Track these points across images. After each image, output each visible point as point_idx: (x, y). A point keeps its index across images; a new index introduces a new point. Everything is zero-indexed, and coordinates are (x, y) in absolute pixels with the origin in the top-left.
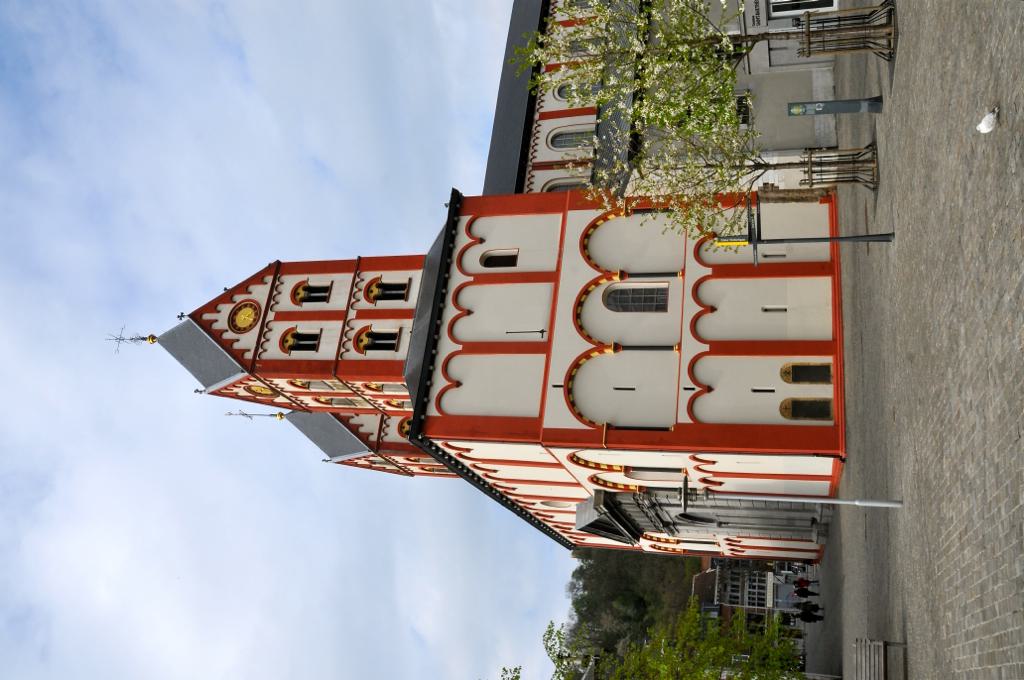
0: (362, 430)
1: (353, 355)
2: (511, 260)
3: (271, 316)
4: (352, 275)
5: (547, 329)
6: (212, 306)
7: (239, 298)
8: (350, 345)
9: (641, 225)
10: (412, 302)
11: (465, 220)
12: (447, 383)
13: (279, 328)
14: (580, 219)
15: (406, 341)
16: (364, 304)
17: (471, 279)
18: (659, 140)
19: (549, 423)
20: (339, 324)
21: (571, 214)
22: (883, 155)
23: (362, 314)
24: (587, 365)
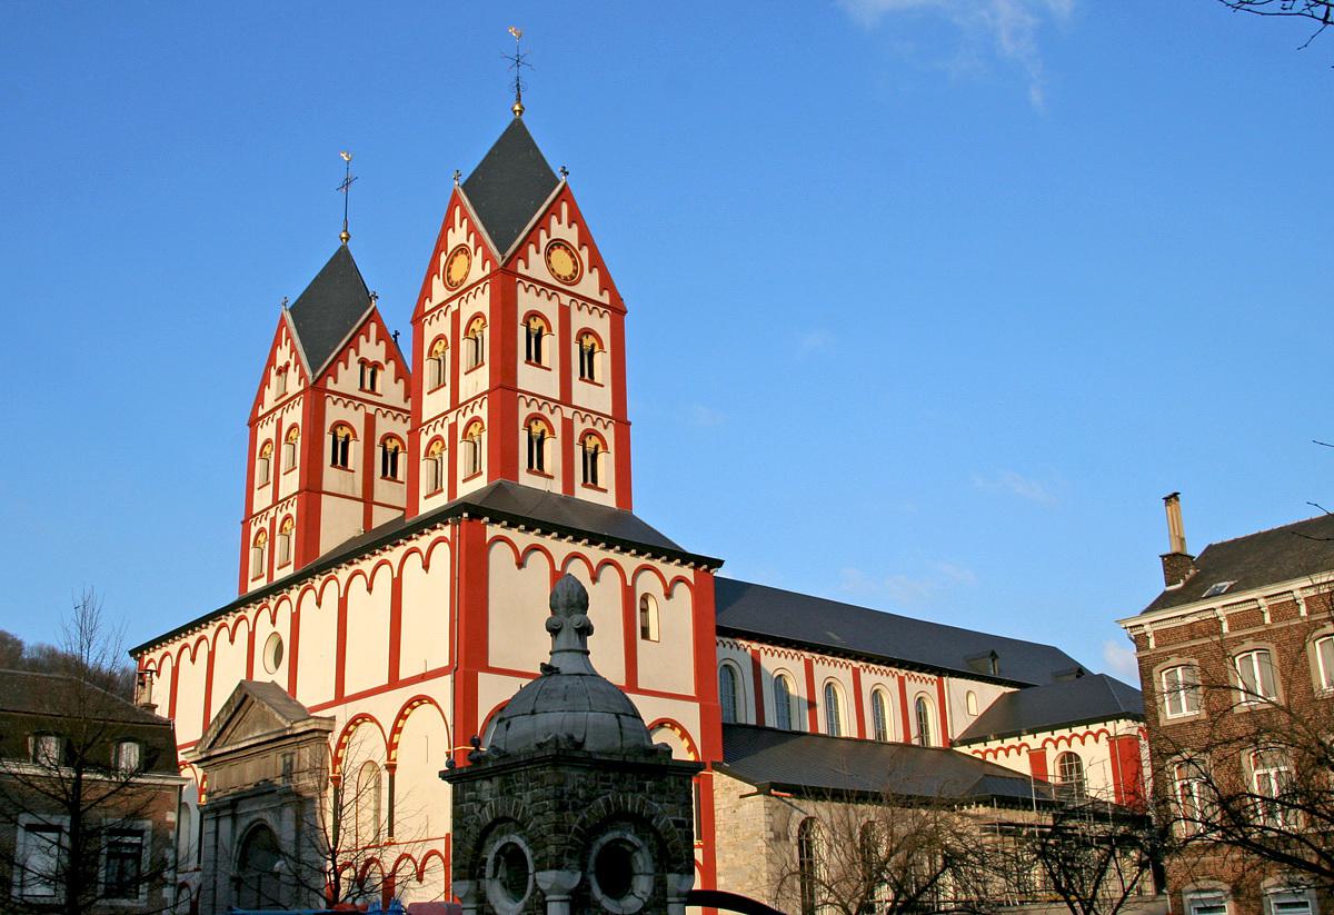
1: (524, 412)
2: (645, 634)
3: (566, 299)
6: (575, 218)
7: (584, 254)
8: (534, 409)
9: (427, 737)
10: (583, 494)
11: (688, 572)
12: (521, 550)
13: (550, 310)
16: (579, 428)
17: (629, 583)
18: (891, 850)
21: (696, 706)
23: (568, 425)
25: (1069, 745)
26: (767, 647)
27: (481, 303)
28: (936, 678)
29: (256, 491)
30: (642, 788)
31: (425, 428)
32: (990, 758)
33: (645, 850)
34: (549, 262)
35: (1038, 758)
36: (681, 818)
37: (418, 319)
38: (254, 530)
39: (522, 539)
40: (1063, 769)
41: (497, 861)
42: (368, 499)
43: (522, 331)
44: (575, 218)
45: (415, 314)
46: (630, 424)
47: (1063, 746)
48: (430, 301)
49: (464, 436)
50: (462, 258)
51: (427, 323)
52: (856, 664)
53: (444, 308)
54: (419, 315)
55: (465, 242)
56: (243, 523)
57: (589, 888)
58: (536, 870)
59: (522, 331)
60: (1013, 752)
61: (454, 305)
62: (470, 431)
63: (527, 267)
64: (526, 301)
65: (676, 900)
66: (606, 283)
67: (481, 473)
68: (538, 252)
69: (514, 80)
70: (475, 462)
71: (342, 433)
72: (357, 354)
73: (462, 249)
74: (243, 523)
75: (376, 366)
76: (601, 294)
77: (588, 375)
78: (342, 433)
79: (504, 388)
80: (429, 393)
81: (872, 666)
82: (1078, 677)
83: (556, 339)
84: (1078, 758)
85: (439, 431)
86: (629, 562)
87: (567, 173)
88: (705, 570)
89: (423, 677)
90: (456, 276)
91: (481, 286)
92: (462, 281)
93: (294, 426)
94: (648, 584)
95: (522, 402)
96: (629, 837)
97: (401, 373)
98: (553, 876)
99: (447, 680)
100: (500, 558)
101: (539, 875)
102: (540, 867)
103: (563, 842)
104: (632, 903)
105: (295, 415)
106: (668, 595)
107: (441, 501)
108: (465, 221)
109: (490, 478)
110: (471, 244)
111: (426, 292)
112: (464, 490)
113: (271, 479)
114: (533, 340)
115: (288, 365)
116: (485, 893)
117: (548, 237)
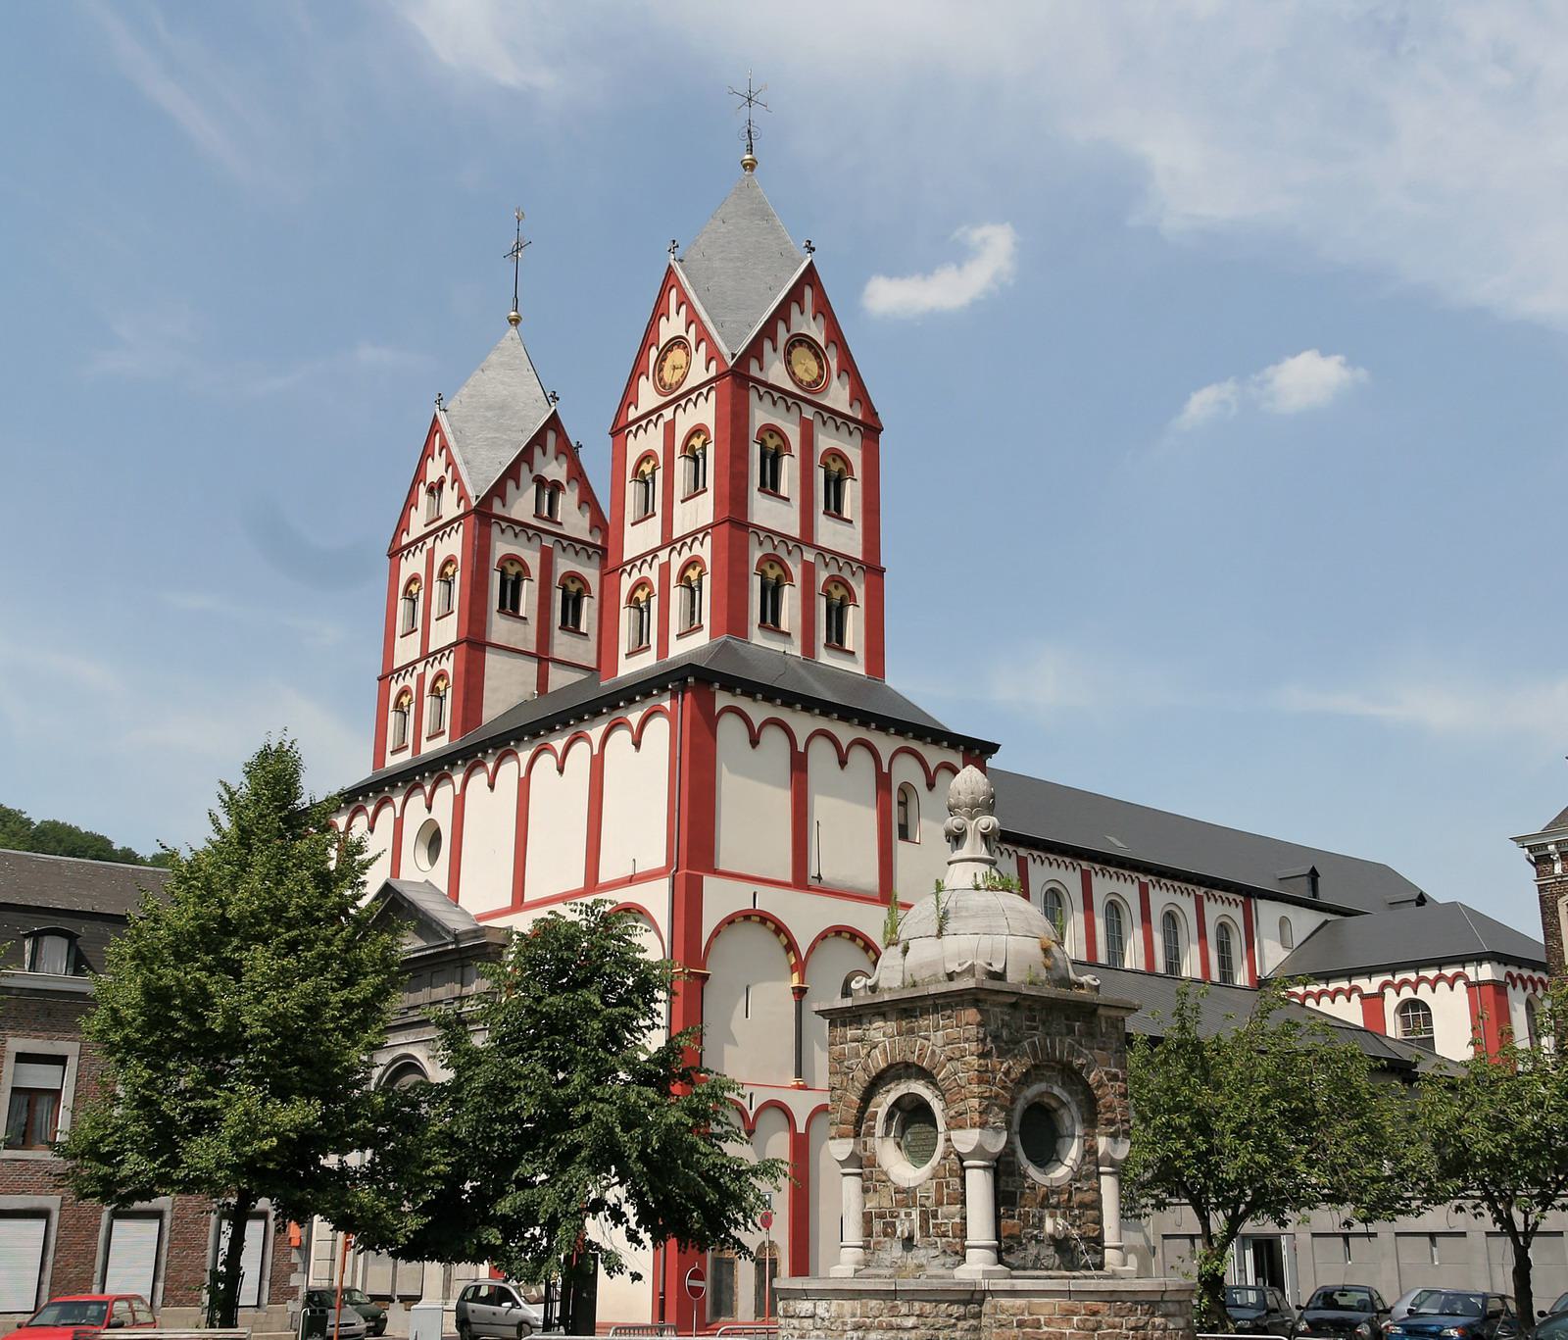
0: (511, 485)
1: (756, 554)
2: (904, 835)
3: (548, 542)
4: (860, 557)
5: (822, 885)
6: (824, 309)
15: (776, 645)
16: (822, 576)
19: (710, 883)
20: (795, 532)
23: (809, 570)
24: (776, 945)
25: (1416, 992)
26: (1036, 853)
27: (705, 412)
28: (1242, 899)
29: (398, 639)
30: (1071, 1031)
31: (628, 568)
32: (1310, 1003)
33: (1074, 1108)
34: (788, 363)
35: (1373, 1003)
36: (1114, 1070)
37: (620, 430)
38: (395, 689)
39: (759, 712)
40: (1405, 1022)
41: (890, 1116)
42: (543, 657)
45: (616, 420)
46: (883, 570)
47: (1407, 993)
48: (636, 408)
49: (396, 706)
50: (677, 356)
51: (631, 436)
52: (1144, 879)
53: (654, 418)
54: (620, 426)
55: (684, 335)
56: (380, 679)
57: (1014, 1152)
58: (949, 1127)
60: (1341, 999)
61: (668, 413)
62: (446, 570)
63: (761, 369)
64: (761, 415)
65: (1110, 1169)
67: (700, 627)
68: (775, 350)
69: (744, 123)
70: (692, 614)
71: (513, 570)
72: (531, 471)
73: (678, 342)
74: (380, 679)
75: (556, 487)
77: (834, 509)
78: (513, 570)
79: (733, 521)
80: (633, 525)
81: (1163, 881)
82: (1418, 904)
83: (797, 461)
84: (1427, 1008)
85: (646, 571)
86: (886, 744)
87: (814, 249)
88: (977, 756)
89: (631, 880)
90: (669, 376)
91: (704, 391)
92: (680, 384)
93: (449, 561)
94: (907, 771)
95: (753, 540)
96: (1056, 1090)
97: (588, 499)
98: (977, 1137)
99: (664, 884)
100: (730, 732)
101: (955, 1134)
102: (957, 1122)
103: (987, 1094)
104: (1061, 1173)
105: (452, 545)
106: (931, 785)
107: (647, 661)
108: (684, 308)
109: (712, 635)
110: (692, 338)
111: (629, 397)
112: (679, 649)
113: (419, 625)
115: (442, 481)
116: (874, 1154)
117: (788, 331)
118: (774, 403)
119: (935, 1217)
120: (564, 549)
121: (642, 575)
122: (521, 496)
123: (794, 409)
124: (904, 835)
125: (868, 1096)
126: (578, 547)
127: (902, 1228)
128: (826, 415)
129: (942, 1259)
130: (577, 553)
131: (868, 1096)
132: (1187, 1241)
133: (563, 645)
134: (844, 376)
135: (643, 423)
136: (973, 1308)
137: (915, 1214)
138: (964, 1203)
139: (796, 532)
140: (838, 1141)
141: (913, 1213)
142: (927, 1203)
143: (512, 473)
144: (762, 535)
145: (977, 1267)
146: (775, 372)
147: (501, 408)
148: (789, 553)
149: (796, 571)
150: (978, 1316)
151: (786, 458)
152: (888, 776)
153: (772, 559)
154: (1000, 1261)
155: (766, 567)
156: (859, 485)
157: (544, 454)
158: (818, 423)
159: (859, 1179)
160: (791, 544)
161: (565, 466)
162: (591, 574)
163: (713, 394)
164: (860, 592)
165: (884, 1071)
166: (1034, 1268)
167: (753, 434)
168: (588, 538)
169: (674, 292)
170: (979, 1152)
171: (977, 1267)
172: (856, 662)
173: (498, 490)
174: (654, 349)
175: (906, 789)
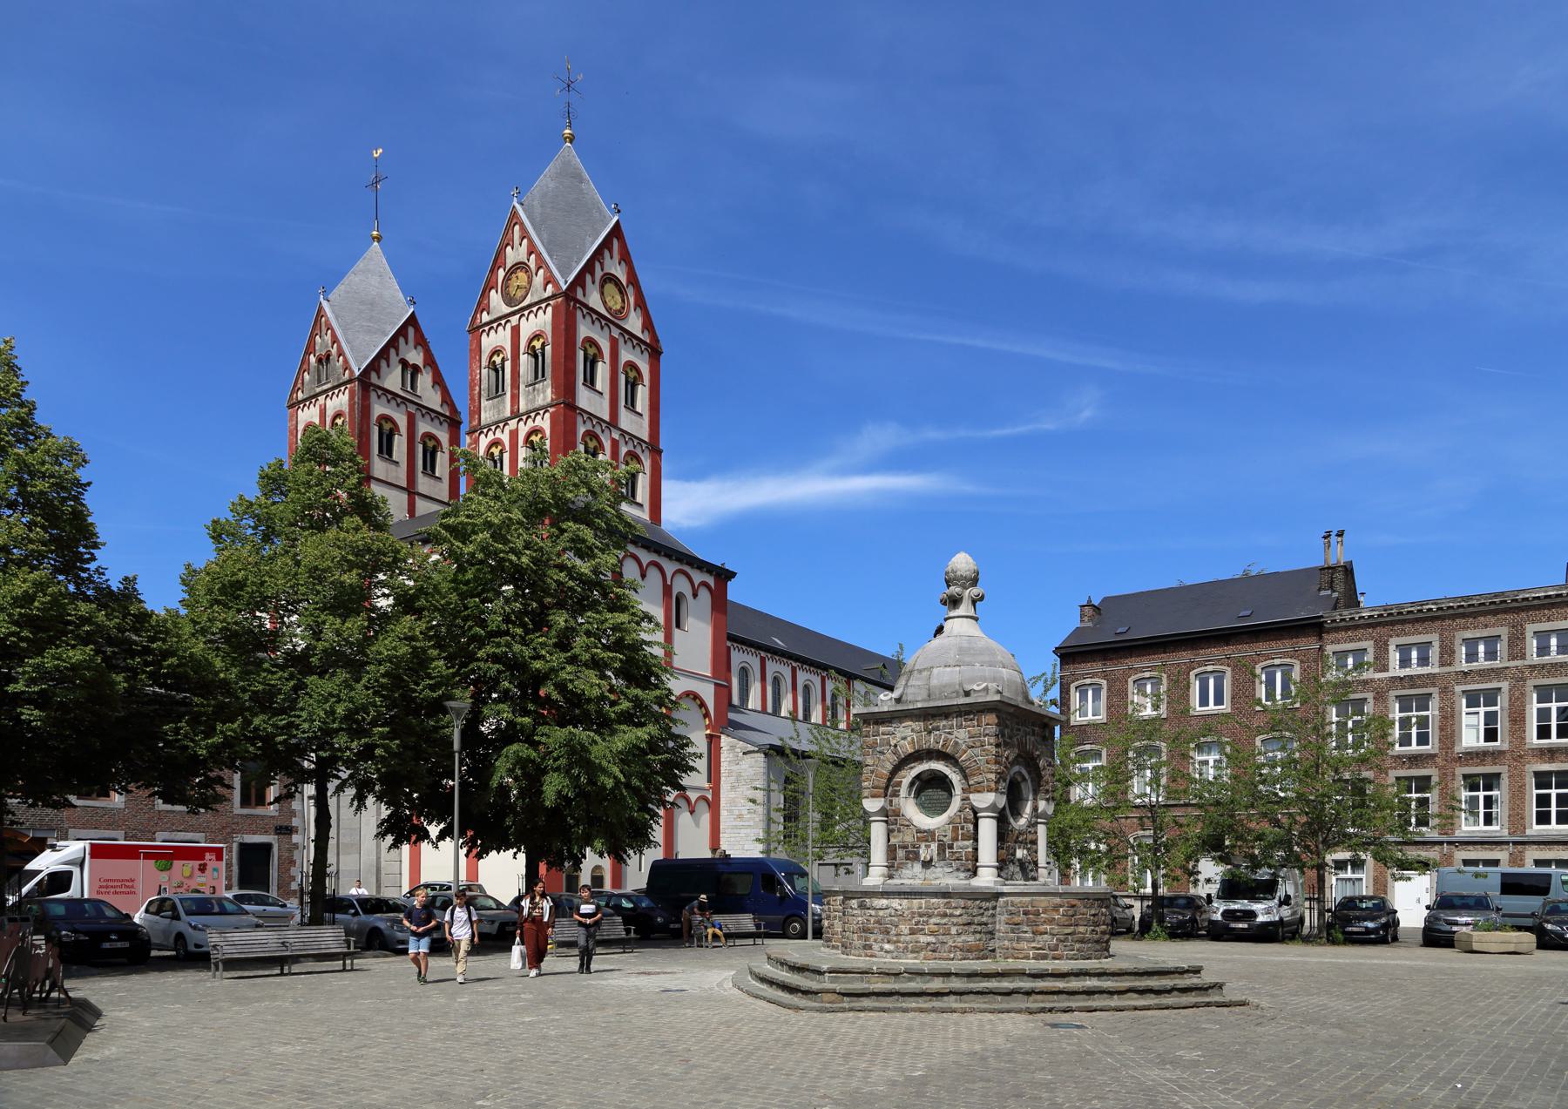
0: (383, 364)
1: (581, 430)
2: (678, 626)
4: (647, 440)
6: (626, 258)
11: (711, 581)
14: (707, 692)
16: (623, 450)
22: (61, 1071)
23: (615, 444)
26: (735, 645)
31: (485, 431)
34: (602, 294)
41: (912, 784)
42: (411, 491)
43: (580, 355)
44: (626, 258)
53: (503, 322)
59: (580, 355)
61: (514, 320)
63: (584, 295)
66: (648, 325)
68: (593, 283)
72: (397, 354)
73: (520, 266)
75: (416, 370)
76: (643, 332)
78: (387, 426)
83: (607, 367)
85: (498, 434)
86: (670, 567)
93: (338, 415)
94: (681, 586)
104: (1023, 821)
106: (695, 595)
108: (525, 241)
111: (483, 306)
114: (588, 364)
117: (602, 270)
118: (593, 322)
119: (951, 847)
120: (423, 416)
121: (536, 423)
122: (391, 373)
123: (606, 328)
124: (678, 626)
125: (897, 769)
126: (433, 415)
127: (924, 854)
128: (627, 337)
129: (956, 874)
130: (432, 420)
131: (897, 769)
132: (833, 867)
133: (423, 484)
134: (638, 309)
135: (495, 325)
136: (993, 903)
137: (934, 846)
138: (976, 840)
139: (606, 417)
140: (870, 799)
141: (933, 847)
142: (945, 839)
143: (384, 354)
144: (586, 416)
145: (987, 878)
146: (594, 300)
147: (371, 304)
148: (603, 431)
149: (607, 445)
150: (994, 908)
151: (600, 364)
152: (671, 586)
153: (591, 435)
154: (999, 876)
155: (588, 439)
156: (647, 389)
157: (407, 343)
158: (621, 341)
159: (883, 824)
160: (604, 425)
161: (422, 354)
162: (443, 436)
163: (550, 310)
164: (647, 463)
165: (911, 754)
166: (1011, 879)
167: (579, 343)
168: (439, 409)
169: (517, 227)
170: (992, 808)
171: (987, 878)
172: (643, 511)
173: (374, 366)
174: (501, 271)
175: (680, 598)
